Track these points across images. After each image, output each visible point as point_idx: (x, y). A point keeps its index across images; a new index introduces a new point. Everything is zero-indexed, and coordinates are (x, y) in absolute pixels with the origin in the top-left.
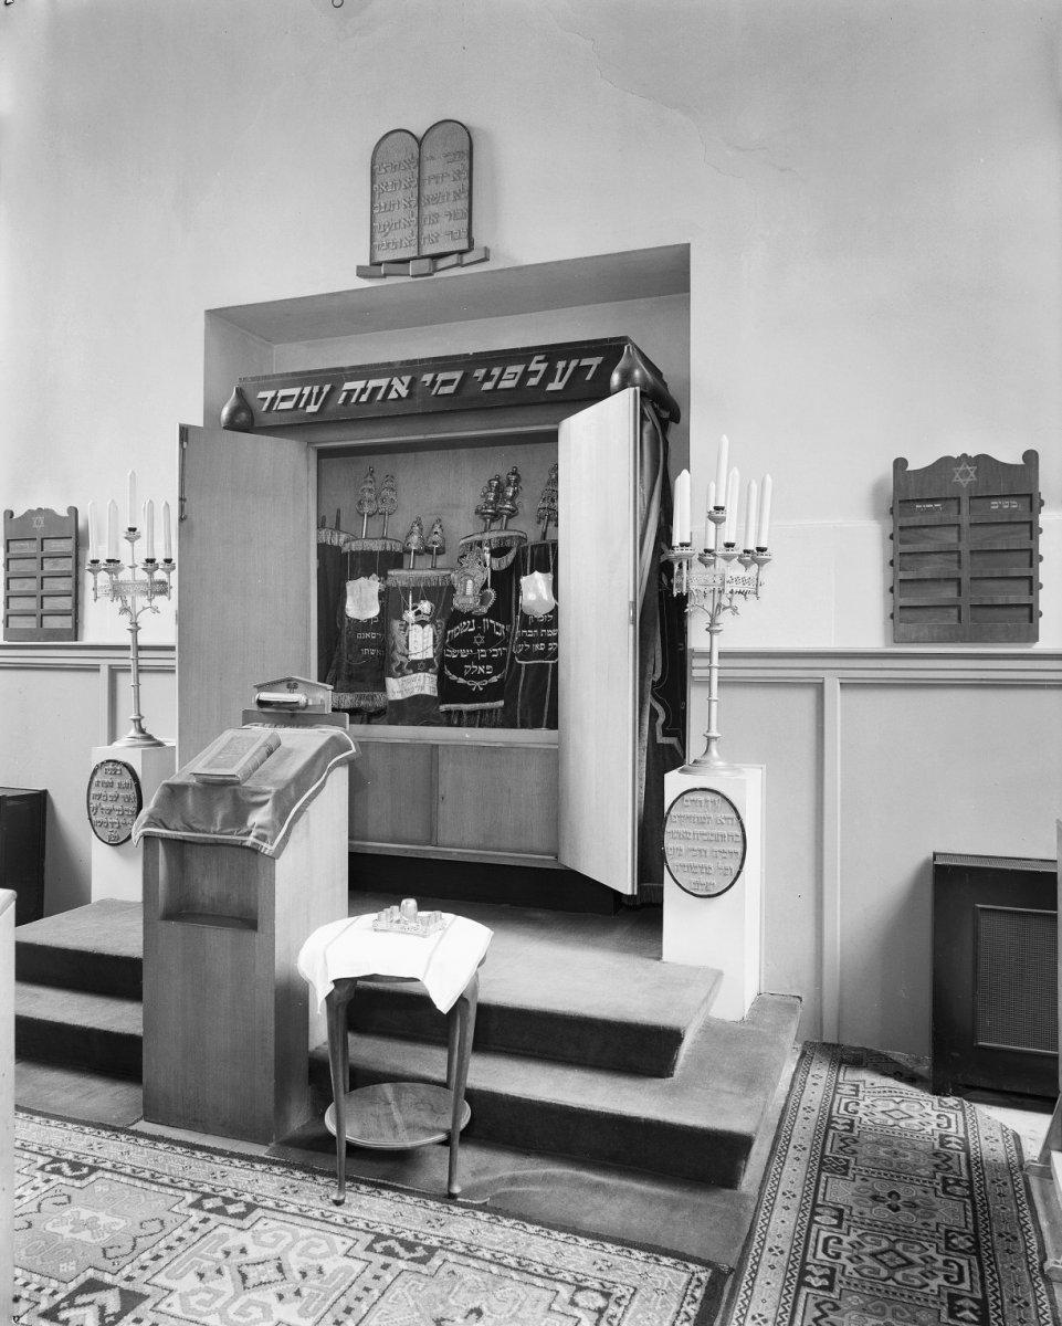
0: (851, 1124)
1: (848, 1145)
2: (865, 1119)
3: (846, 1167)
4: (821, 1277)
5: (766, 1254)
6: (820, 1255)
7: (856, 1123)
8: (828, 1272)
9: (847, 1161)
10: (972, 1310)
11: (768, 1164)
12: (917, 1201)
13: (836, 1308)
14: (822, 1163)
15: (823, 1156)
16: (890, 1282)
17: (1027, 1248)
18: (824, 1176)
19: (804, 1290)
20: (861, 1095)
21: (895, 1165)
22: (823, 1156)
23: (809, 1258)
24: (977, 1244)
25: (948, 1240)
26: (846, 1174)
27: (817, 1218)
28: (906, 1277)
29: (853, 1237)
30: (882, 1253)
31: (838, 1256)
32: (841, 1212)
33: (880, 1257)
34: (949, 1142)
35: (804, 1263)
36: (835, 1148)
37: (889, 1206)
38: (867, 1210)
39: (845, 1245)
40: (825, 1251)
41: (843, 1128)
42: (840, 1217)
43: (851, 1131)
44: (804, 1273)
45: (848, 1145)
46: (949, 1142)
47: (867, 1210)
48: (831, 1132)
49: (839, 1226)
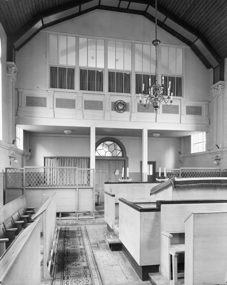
0: (86, 277)
1: (85, 272)
2: (84, 279)
3: (84, 268)
4: (88, 276)
5: (97, 277)
6: (89, 279)
7: (85, 277)
8: (87, 277)
9: (84, 269)
10: (65, 278)
11: (99, 272)
12: (72, 266)
13: (84, 273)
14: (88, 267)
15: (89, 269)
16: (77, 278)
17: (57, 269)
18: (84, 248)
19: (89, 274)
20: (82, 260)
21: (77, 271)
22: (89, 269)
23: (90, 278)
24: (64, 262)
25: (68, 262)
26: (84, 267)
27: (90, 275)
28: (75, 280)
29: (81, 259)
30: (79, 283)
31: (86, 280)
32: (83, 262)
33: (79, 282)
34: (67, 278)
35: (91, 277)
36: (87, 271)
37: (77, 264)
38: (80, 263)
39: (85, 282)
40: (88, 280)
41: (87, 275)
42: (83, 261)
43: (86, 275)
44: (90, 276)
45: (85, 272)
46: (67, 278)
47: (80, 263)
48: (89, 274)
49: (83, 260)
